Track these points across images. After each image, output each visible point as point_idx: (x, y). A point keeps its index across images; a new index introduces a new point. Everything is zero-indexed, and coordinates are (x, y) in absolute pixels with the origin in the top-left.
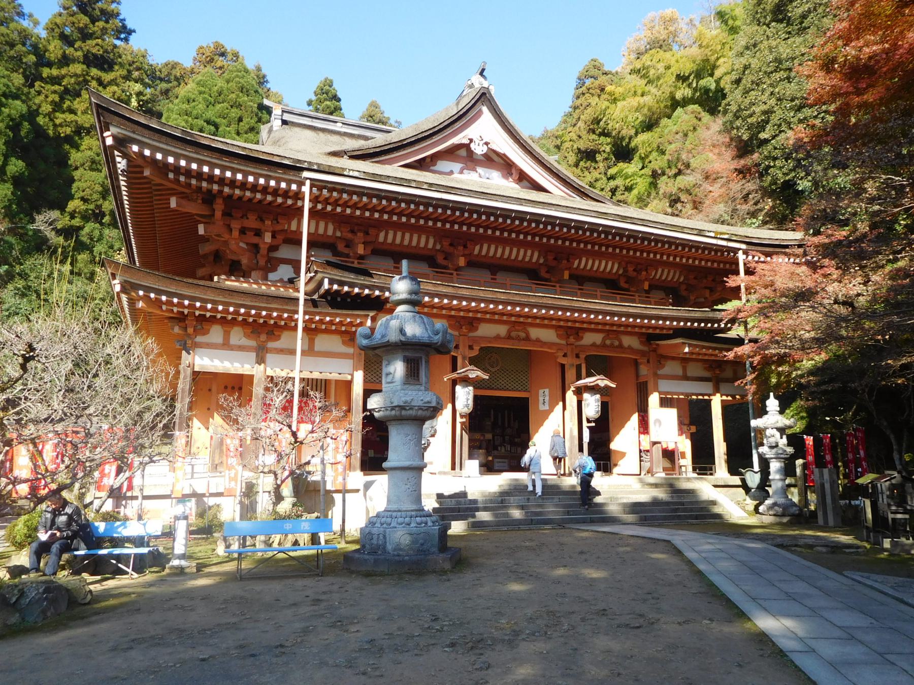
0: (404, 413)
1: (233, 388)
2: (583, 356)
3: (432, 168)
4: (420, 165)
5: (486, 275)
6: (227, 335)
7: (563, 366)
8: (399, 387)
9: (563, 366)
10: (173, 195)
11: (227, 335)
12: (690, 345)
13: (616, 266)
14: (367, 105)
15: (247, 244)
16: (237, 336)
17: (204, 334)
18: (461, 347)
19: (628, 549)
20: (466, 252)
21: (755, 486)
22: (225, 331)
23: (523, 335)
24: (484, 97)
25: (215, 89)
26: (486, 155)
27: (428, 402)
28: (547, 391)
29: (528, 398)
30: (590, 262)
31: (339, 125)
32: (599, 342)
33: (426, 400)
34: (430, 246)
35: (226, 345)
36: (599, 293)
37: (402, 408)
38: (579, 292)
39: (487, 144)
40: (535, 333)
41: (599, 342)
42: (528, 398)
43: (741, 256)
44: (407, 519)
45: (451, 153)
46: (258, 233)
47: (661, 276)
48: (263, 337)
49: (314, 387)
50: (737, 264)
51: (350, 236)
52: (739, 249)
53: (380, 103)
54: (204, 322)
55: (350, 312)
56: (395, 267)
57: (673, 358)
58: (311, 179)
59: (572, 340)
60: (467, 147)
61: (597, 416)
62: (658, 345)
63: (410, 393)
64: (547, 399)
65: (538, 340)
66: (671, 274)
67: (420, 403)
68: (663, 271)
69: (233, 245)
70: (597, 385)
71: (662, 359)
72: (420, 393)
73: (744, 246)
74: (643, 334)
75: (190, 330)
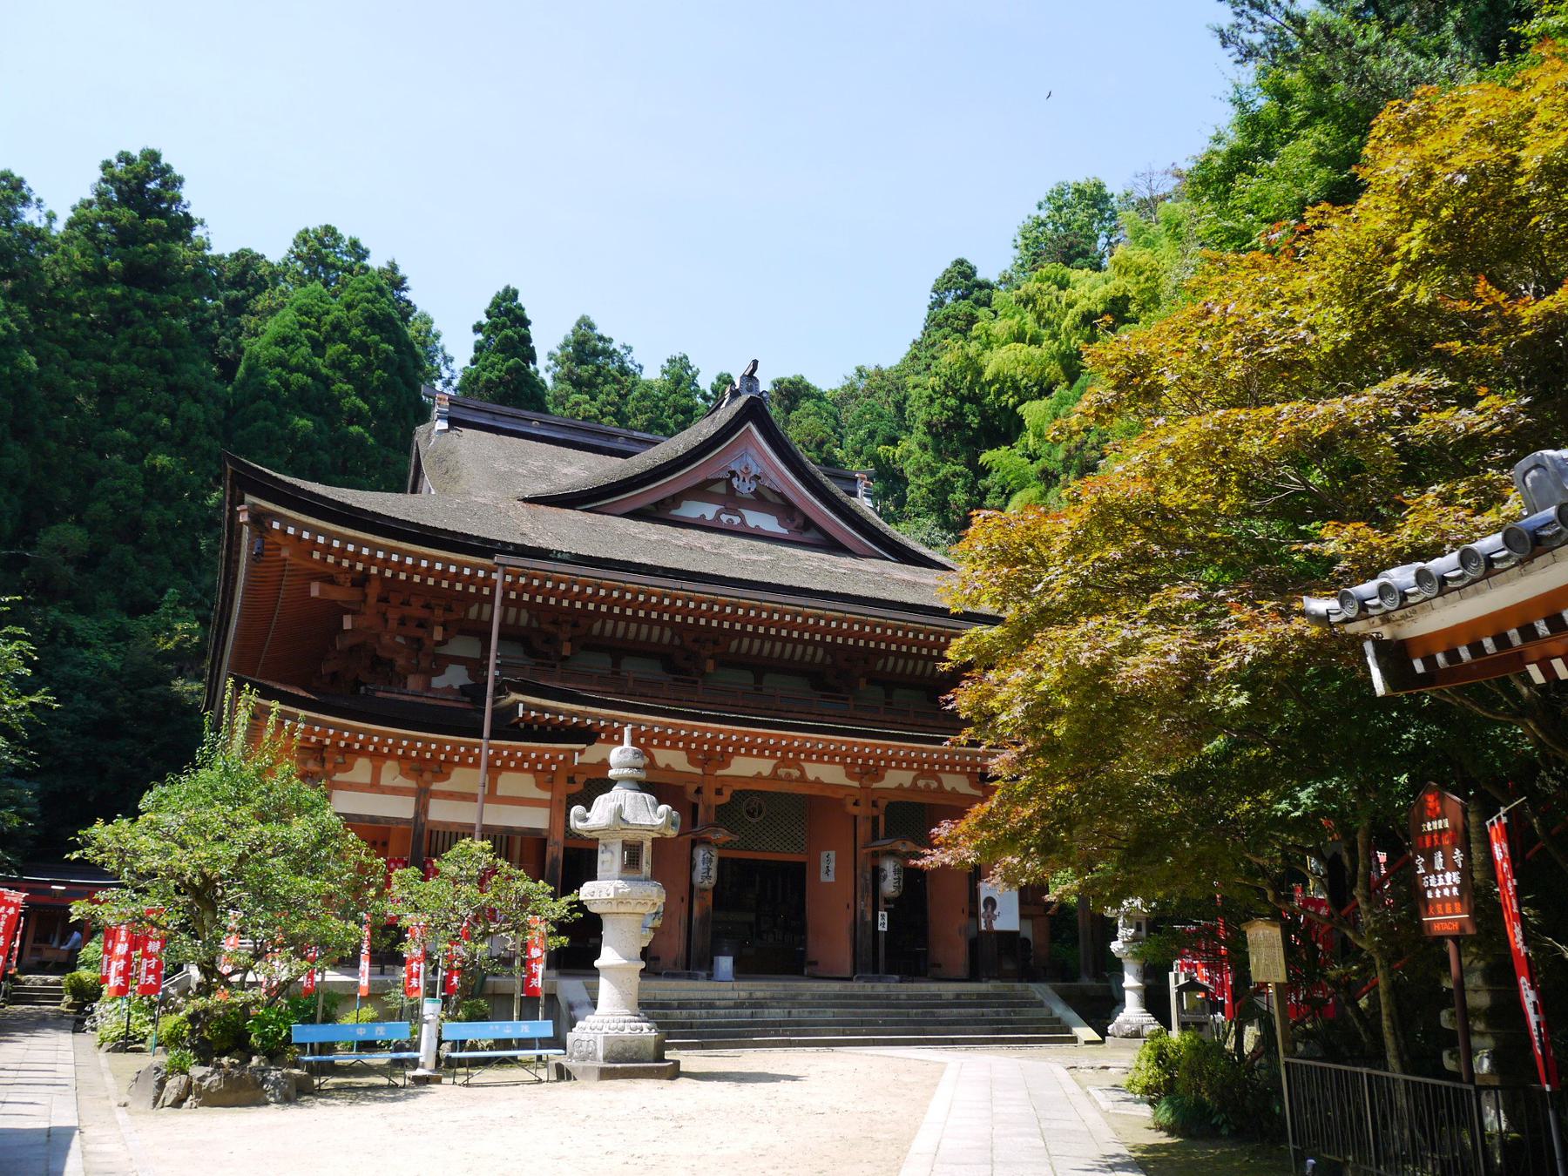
2: (883, 804)
3: (674, 512)
4: (656, 513)
6: (376, 774)
11: (376, 774)
14: (572, 324)
15: (406, 638)
18: (705, 790)
23: (796, 773)
25: (329, 318)
28: (833, 854)
29: (803, 864)
35: (375, 786)
39: (757, 477)
40: (813, 771)
41: (907, 784)
45: (701, 491)
53: (594, 319)
61: (897, 894)
64: (832, 866)
65: (818, 781)
69: (386, 639)
75: (329, 766)
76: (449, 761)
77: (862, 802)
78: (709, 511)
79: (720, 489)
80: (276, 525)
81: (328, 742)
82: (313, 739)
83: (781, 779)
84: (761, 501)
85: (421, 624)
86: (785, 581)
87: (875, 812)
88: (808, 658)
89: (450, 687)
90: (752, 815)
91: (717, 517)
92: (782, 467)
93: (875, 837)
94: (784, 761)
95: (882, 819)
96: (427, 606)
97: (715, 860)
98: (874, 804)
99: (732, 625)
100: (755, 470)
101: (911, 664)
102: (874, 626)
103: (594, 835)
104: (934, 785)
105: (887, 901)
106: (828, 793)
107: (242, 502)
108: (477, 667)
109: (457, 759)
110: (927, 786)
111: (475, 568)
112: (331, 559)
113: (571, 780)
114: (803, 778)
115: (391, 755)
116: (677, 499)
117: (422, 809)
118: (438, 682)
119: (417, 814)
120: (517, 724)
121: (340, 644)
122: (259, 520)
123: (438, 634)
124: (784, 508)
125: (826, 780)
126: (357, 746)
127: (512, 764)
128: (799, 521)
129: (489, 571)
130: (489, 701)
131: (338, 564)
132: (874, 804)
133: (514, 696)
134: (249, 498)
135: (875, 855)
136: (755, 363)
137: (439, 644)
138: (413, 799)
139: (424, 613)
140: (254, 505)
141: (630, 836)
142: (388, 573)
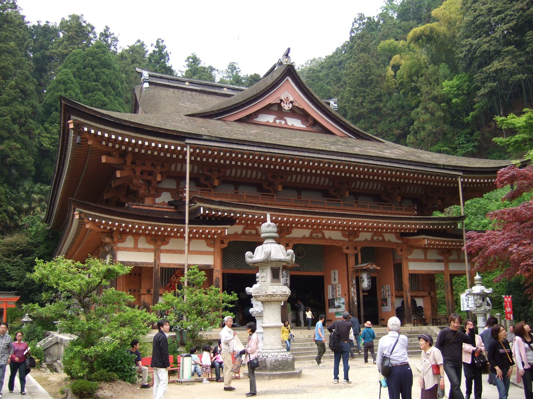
0: (272, 298)
1: (135, 274)
2: (359, 248)
3: (255, 120)
4: (247, 120)
5: (293, 194)
6: (136, 243)
7: (347, 255)
8: (269, 284)
10: (103, 155)
11: (136, 243)
12: (428, 239)
15: (143, 180)
16: (142, 243)
17: (123, 242)
21: (442, 362)
22: (135, 240)
23: (320, 235)
27: (285, 292)
28: (337, 271)
29: (322, 277)
31: (187, 83)
32: (369, 238)
33: (283, 291)
34: (259, 177)
35: (136, 249)
37: (272, 296)
38: (355, 204)
39: (292, 102)
40: (328, 234)
41: (369, 238)
43: (460, 180)
44: (276, 354)
45: (267, 109)
47: (413, 192)
48: (159, 243)
49: (167, 269)
51: (209, 173)
52: (459, 175)
54: (123, 234)
55: (214, 226)
57: (418, 248)
58: (190, 144)
60: (279, 105)
61: (369, 288)
62: (408, 239)
63: (275, 287)
64: (337, 277)
65: (330, 239)
66: (416, 189)
67: (281, 293)
69: (135, 181)
70: (369, 268)
71: (411, 248)
72: (281, 287)
73: (461, 174)
75: (115, 240)
76: (169, 236)
79: (275, 108)
80: (86, 129)
81: (115, 229)
82: (108, 228)
83: (247, 235)
85: (150, 174)
86: (234, 137)
87: (356, 252)
88: (322, 183)
89: (164, 202)
91: (275, 122)
92: (303, 97)
93: (357, 263)
94: (375, 234)
95: (359, 255)
96: (153, 165)
97: (289, 276)
98: (356, 248)
99: (231, 162)
100: (291, 99)
101: (249, 172)
102: (309, 162)
103: (256, 265)
104: (320, 235)
106: (335, 244)
108: (178, 193)
109: (172, 234)
110: (378, 239)
112: (110, 145)
113: (222, 242)
114: (323, 237)
115: (140, 235)
116: (256, 114)
117: (157, 258)
118: (158, 200)
119: (155, 260)
120: (199, 218)
121: (114, 184)
122: (78, 127)
123: (159, 178)
124: (304, 115)
125: (334, 238)
126: (128, 230)
127: (197, 236)
128: (311, 122)
129: (183, 147)
130: (187, 207)
131: (113, 147)
133: (198, 204)
134: (72, 117)
136: (289, 50)
137: (159, 182)
138: (153, 254)
140: (75, 120)
141: (274, 265)
142: (137, 150)
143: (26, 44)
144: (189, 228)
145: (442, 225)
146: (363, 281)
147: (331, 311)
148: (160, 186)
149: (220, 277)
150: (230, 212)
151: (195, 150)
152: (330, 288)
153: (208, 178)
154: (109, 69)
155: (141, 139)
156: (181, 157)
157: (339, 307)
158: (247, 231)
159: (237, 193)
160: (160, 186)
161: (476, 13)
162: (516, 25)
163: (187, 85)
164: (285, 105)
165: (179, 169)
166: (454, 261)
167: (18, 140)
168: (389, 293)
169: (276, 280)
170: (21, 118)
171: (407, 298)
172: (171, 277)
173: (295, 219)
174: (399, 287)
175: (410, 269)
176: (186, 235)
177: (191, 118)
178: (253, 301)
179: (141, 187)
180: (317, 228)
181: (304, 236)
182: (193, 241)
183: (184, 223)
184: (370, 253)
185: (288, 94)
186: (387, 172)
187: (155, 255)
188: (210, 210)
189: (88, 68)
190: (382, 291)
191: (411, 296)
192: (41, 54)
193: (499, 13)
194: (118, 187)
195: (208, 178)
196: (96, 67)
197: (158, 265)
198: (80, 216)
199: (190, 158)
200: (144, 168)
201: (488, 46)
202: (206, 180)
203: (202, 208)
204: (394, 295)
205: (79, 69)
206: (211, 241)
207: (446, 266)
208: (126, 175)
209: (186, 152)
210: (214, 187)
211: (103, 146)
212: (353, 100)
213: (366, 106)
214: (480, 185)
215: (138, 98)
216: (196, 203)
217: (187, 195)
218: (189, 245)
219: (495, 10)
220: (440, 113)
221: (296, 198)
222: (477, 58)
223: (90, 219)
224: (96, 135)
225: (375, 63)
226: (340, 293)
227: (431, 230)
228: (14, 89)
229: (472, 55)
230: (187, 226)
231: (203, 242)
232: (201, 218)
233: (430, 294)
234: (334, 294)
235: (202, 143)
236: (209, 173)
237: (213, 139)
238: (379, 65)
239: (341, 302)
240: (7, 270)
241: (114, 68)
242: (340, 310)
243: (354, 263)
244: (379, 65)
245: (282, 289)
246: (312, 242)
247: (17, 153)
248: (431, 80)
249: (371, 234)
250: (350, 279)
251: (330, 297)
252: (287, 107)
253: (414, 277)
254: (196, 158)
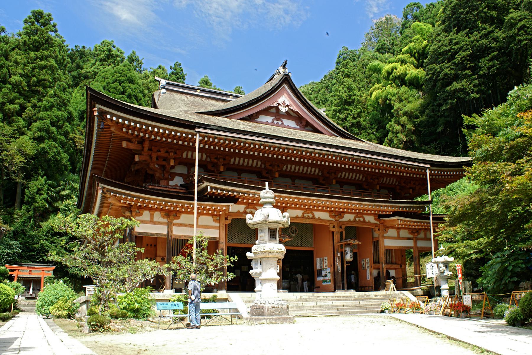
1: (151, 245)
2: (343, 227)
3: (256, 120)
4: (250, 118)
6: (152, 216)
7: (333, 232)
9: (333, 232)
11: (152, 216)
13: (361, 176)
15: (159, 165)
17: (140, 216)
19: (495, 53)
20: (279, 169)
22: (151, 214)
23: (311, 216)
24: (286, 80)
26: (287, 112)
29: (311, 252)
30: (347, 174)
32: (352, 219)
34: (259, 165)
35: (152, 222)
36: (352, 192)
37: (270, 252)
38: (341, 191)
39: (288, 106)
40: (317, 215)
41: (352, 219)
42: (311, 252)
43: (428, 172)
45: (266, 111)
46: (166, 159)
50: (426, 175)
56: (238, 178)
57: (392, 228)
58: (199, 132)
59: (337, 218)
60: (277, 108)
61: (351, 260)
62: (384, 220)
65: (319, 219)
66: (391, 180)
68: (387, 179)
69: (152, 166)
71: (387, 227)
73: (429, 166)
74: (376, 214)
75: (134, 214)
76: (181, 212)
77: (336, 226)
78: (270, 119)
79: (273, 110)
80: (108, 116)
84: (289, 115)
87: (341, 230)
89: (176, 185)
90: (293, 234)
93: (341, 238)
98: (341, 227)
100: (287, 103)
103: (256, 227)
104: (311, 216)
105: (347, 262)
107: (95, 107)
110: (359, 220)
111: (187, 134)
113: (226, 219)
114: (313, 218)
117: (170, 230)
118: (172, 183)
120: (206, 196)
121: (133, 168)
122: (102, 114)
123: (172, 163)
128: (304, 123)
132: (341, 227)
133: (206, 184)
134: (97, 105)
135: (342, 246)
136: (286, 61)
138: (166, 227)
139: (167, 155)
140: (100, 108)
141: (272, 226)
142: (153, 137)
143: (65, 63)
144: (198, 204)
145: (413, 208)
146: (347, 253)
147: (320, 279)
148: (173, 171)
149: (224, 248)
150: (233, 191)
151: (204, 137)
152: (318, 260)
153: (215, 165)
154: (133, 84)
155: (157, 127)
156: (191, 144)
157: (326, 276)
158: (357, 219)
159: (240, 178)
160: (173, 171)
161: (440, 44)
162: (471, 54)
163: (198, 93)
164: (282, 108)
165: (189, 157)
166: (422, 239)
167: (55, 140)
168: (369, 265)
169: (273, 239)
170: (58, 121)
171: (383, 269)
172: (181, 246)
173: (289, 200)
174: (377, 262)
175: (385, 245)
176: (195, 211)
177: (201, 115)
178: (253, 264)
179: (157, 171)
180: (308, 209)
181: (297, 216)
182: (201, 217)
183: (193, 200)
184: (352, 231)
185: (285, 100)
186: (368, 163)
187: (168, 227)
188: (216, 189)
189: (116, 83)
190: (362, 263)
191: (386, 269)
192: (78, 72)
193: (457, 43)
194: (137, 171)
195: (215, 165)
196: (123, 82)
197: (171, 236)
198: (103, 191)
199: (199, 145)
200: (159, 153)
201: (449, 70)
202: (213, 166)
203: (209, 187)
204: (373, 266)
205: (108, 84)
206: (217, 216)
207: (415, 243)
208: (144, 159)
209: (196, 140)
210: (220, 173)
211: (123, 133)
212: (338, 116)
213: (349, 120)
214: (446, 176)
215: (156, 101)
216: (203, 183)
217: (196, 178)
218: (197, 219)
219: (454, 41)
220: (409, 126)
221: (291, 184)
222: (439, 80)
223: (112, 194)
224: (118, 123)
225: (357, 87)
226: (327, 264)
227: (404, 212)
228: (53, 97)
229: (436, 77)
230: (196, 202)
231: (210, 218)
232: (208, 196)
233: (401, 266)
234: (322, 265)
235: (209, 131)
236: (215, 161)
237: (219, 129)
238: (360, 88)
239: (328, 272)
240: (46, 247)
241: (138, 84)
242: (327, 278)
243: (339, 239)
244: (360, 88)
245: (278, 248)
246: (304, 221)
247: (55, 150)
248: (403, 98)
249: (354, 216)
250: (335, 252)
251: (318, 268)
252: (283, 109)
253: (389, 251)
254: (204, 146)
